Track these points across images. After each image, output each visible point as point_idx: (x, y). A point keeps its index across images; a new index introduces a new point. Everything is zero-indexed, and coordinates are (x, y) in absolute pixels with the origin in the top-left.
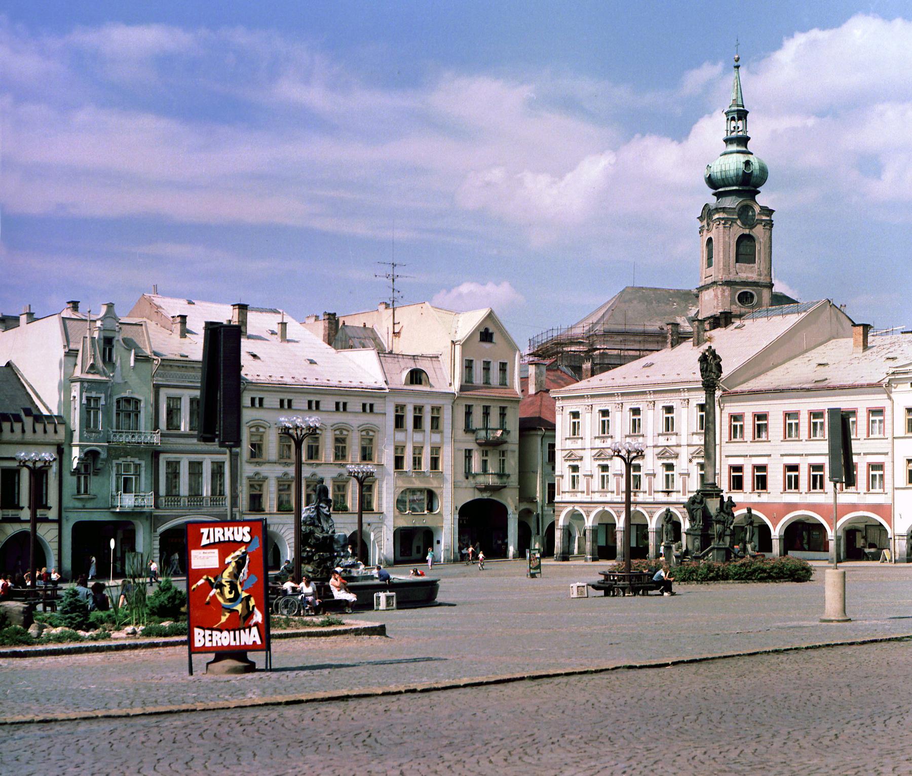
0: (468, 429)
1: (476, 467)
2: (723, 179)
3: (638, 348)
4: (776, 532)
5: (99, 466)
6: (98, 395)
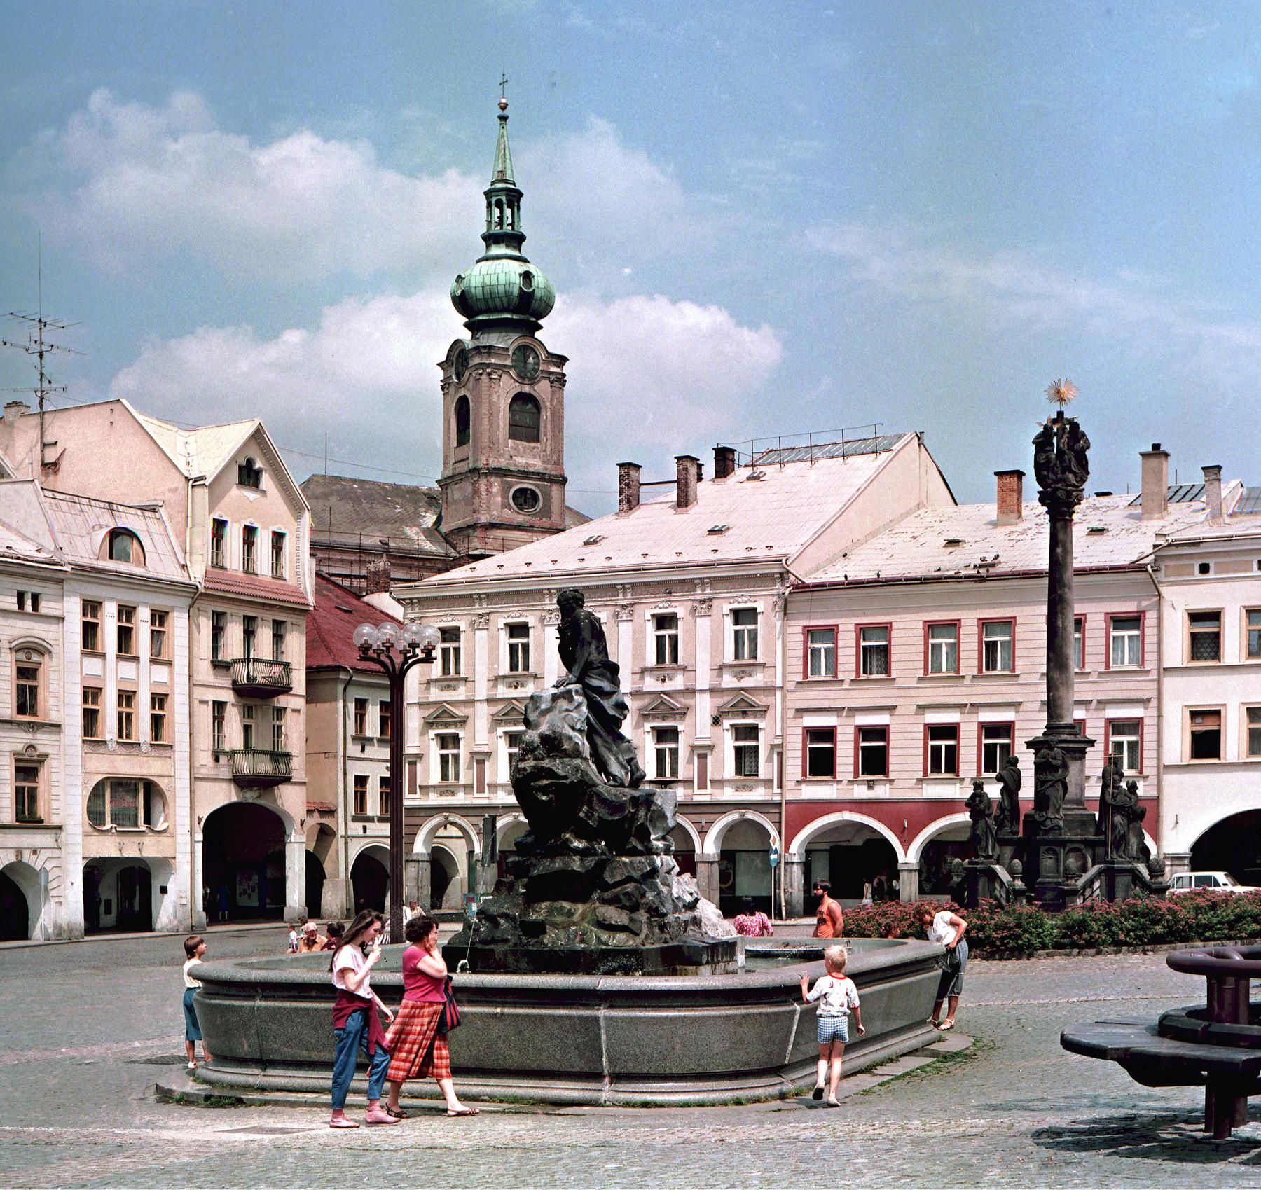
0: (220, 666)
1: (234, 737)
2: (485, 300)
3: (348, 572)
4: (909, 857)
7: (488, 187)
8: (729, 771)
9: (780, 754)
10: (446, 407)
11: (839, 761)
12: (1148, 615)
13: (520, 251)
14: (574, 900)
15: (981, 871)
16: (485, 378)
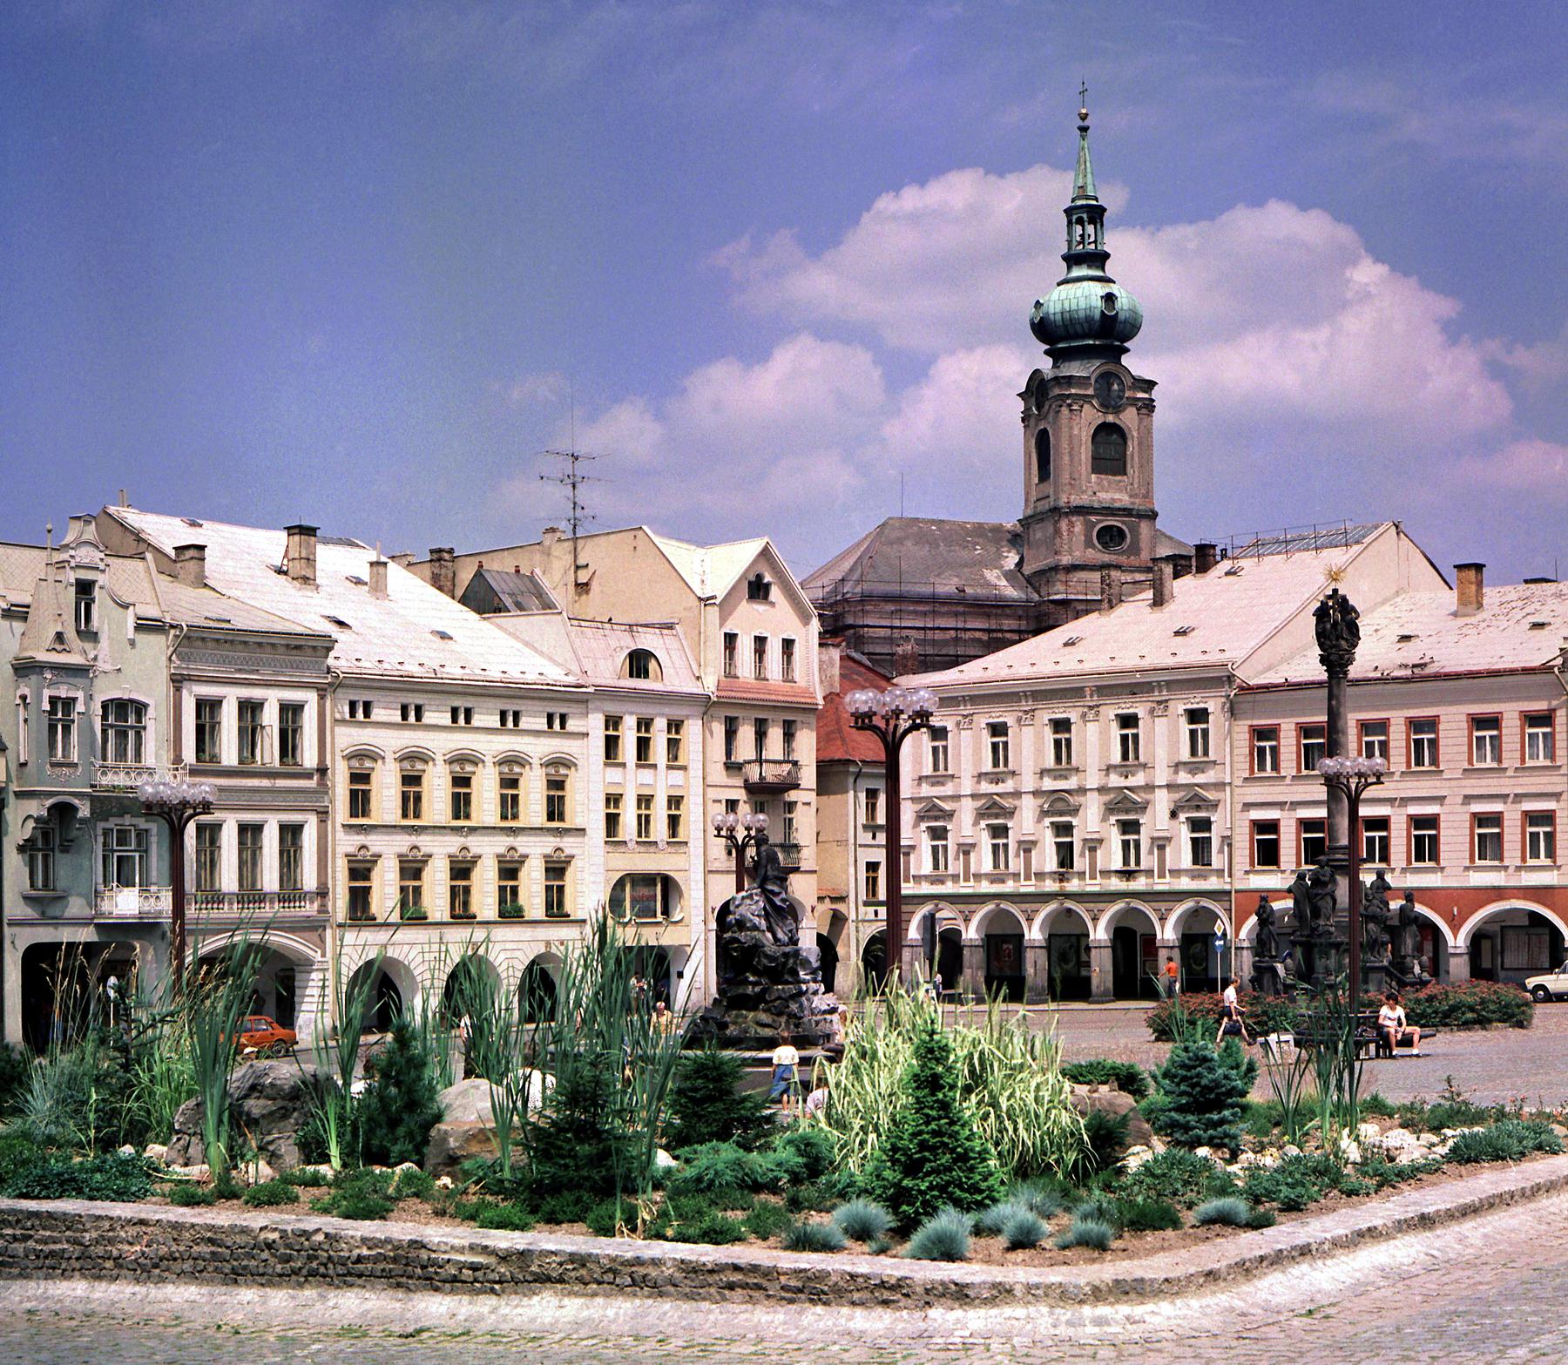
0: (732, 767)
2: (1065, 326)
4: (1457, 941)
5: (74, 834)
6: (71, 694)
7: (1069, 204)
8: (1186, 860)
9: (1230, 845)
10: (1026, 440)
11: (1282, 851)
12: (1558, 713)
13: (1104, 271)
14: (749, 1009)
15: (1265, 968)
16: (1065, 410)
